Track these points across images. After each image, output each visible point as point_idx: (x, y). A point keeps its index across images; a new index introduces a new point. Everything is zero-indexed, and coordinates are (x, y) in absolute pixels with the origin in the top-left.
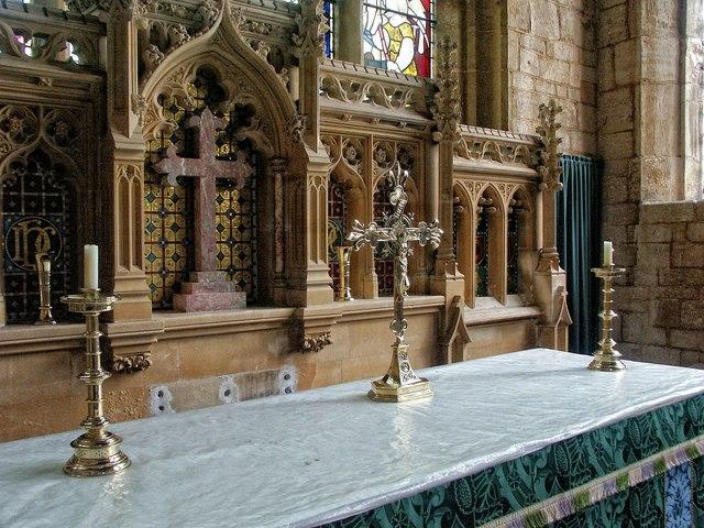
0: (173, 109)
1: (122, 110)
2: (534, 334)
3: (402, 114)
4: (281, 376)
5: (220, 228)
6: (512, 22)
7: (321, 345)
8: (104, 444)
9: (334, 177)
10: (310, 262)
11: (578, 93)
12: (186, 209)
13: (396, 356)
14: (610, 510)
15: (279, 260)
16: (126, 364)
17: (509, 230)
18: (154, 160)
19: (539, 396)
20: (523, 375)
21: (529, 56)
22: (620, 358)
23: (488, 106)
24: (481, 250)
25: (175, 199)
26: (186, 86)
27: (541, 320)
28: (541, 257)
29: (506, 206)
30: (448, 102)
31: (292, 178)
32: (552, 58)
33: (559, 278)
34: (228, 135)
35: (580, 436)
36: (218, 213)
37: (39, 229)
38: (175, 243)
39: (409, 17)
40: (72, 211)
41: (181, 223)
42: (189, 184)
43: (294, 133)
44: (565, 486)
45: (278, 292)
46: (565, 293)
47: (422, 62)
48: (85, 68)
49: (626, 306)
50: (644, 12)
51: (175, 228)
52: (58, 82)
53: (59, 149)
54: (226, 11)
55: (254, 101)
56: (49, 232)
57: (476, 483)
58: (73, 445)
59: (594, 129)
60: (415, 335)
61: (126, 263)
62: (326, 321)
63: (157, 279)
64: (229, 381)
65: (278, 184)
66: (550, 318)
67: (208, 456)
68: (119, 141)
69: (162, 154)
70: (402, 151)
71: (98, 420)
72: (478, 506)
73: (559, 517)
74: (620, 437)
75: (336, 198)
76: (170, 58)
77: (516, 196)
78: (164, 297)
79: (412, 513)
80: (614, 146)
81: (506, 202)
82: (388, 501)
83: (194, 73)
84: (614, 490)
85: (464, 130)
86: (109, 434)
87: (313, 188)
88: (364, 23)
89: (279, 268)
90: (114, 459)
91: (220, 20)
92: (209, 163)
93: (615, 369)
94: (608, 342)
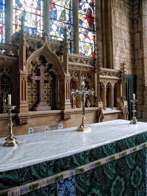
0: (34, 65)
1: (22, 65)
2: (120, 116)
3: (88, 65)
4: (59, 126)
5: (45, 92)
6: (114, 44)
7: (69, 119)
8: (12, 140)
9: (72, 80)
10: (66, 100)
11: (130, 60)
12: (37, 88)
13: (83, 121)
14: (132, 156)
15: (59, 99)
16: (23, 123)
17: (114, 92)
18: (30, 76)
19: (116, 130)
20: (114, 125)
21: (118, 52)
22: (137, 121)
23: (109, 64)
24: (107, 97)
25: (35, 85)
26: (37, 59)
27: (122, 113)
28: (121, 98)
29: (113, 86)
30: (99, 63)
31: (62, 80)
32: (124, 52)
33: (126, 103)
34: (47, 70)
35: (124, 139)
36: (44, 89)
37: (4, 92)
38: (35, 95)
39: (90, 44)
40: (11, 88)
41: (36, 91)
42: (38, 82)
43: (62, 70)
44: (120, 151)
45: (58, 107)
46: (127, 107)
47: (94, 54)
48: (14, 56)
49: (142, 110)
50: (144, 42)
51: (35, 92)
52: (8, 60)
53: (8, 74)
54: (46, 43)
55: (53, 63)
56: (6, 93)
57: (98, 150)
58: (5, 140)
59: (134, 69)
60: (91, 116)
61: (23, 100)
62: (70, 113)
63: (30, 103)
64: (47, 127)
65: (58, 82)
66: (124, 113)
67: (36, 143)
68: (21, 72)
69: (32, 75)
70: (88, 74)
71: (11, 134)
72: (98, 155)
73: (119, 158)
74: (134, 139)
75: (72, 85)
76: (33, 53)
77: (115, 84)
78: (32, 108)
79: (81, 157)
80: (139, 73)
81: (113, 85)
82: (75, 153)
83: (39, 56)
84: (133, 152)
85: (102, 69)
86: (14, 137)
87: (66, 82)
88: (80, 46)
89: (59, 101)
90: (15, 143)
91: (44, 45)
92: (42, 77)
93: (136, 124)
94: (134, 117)
